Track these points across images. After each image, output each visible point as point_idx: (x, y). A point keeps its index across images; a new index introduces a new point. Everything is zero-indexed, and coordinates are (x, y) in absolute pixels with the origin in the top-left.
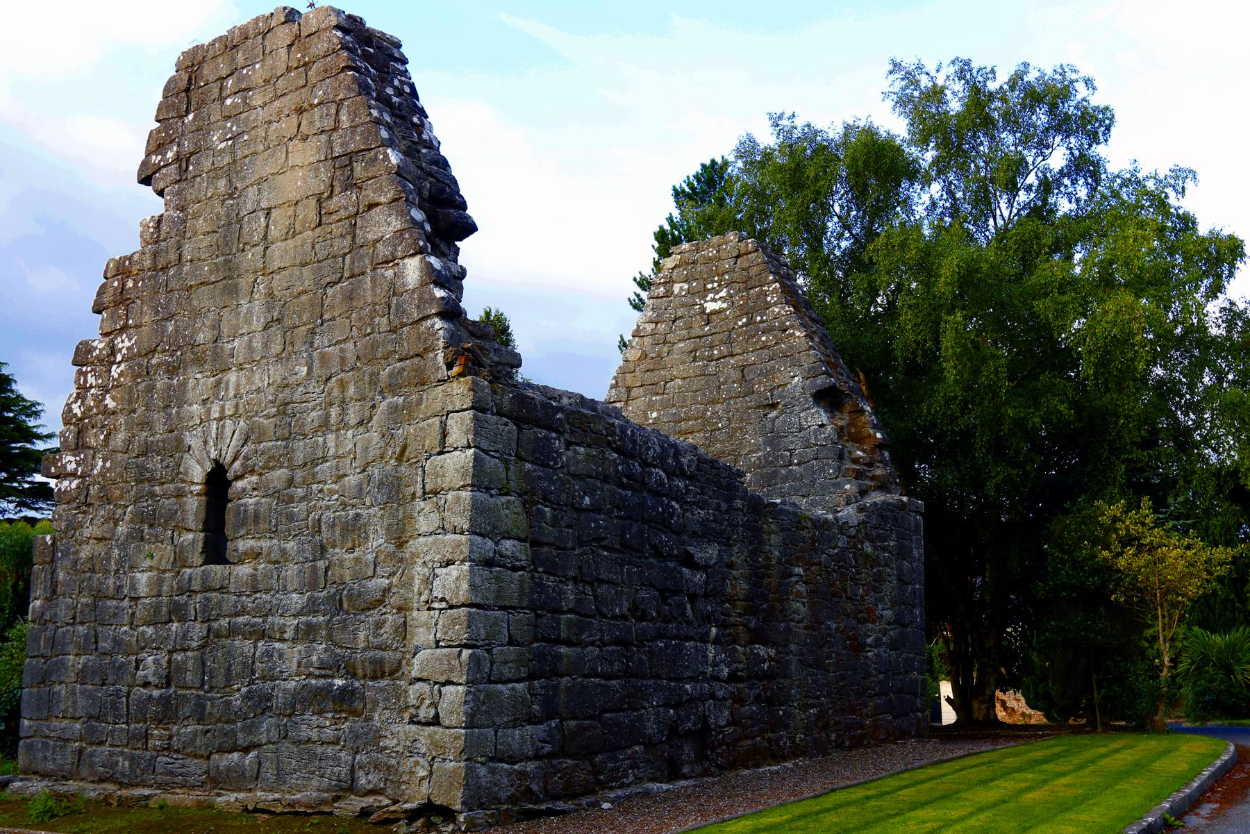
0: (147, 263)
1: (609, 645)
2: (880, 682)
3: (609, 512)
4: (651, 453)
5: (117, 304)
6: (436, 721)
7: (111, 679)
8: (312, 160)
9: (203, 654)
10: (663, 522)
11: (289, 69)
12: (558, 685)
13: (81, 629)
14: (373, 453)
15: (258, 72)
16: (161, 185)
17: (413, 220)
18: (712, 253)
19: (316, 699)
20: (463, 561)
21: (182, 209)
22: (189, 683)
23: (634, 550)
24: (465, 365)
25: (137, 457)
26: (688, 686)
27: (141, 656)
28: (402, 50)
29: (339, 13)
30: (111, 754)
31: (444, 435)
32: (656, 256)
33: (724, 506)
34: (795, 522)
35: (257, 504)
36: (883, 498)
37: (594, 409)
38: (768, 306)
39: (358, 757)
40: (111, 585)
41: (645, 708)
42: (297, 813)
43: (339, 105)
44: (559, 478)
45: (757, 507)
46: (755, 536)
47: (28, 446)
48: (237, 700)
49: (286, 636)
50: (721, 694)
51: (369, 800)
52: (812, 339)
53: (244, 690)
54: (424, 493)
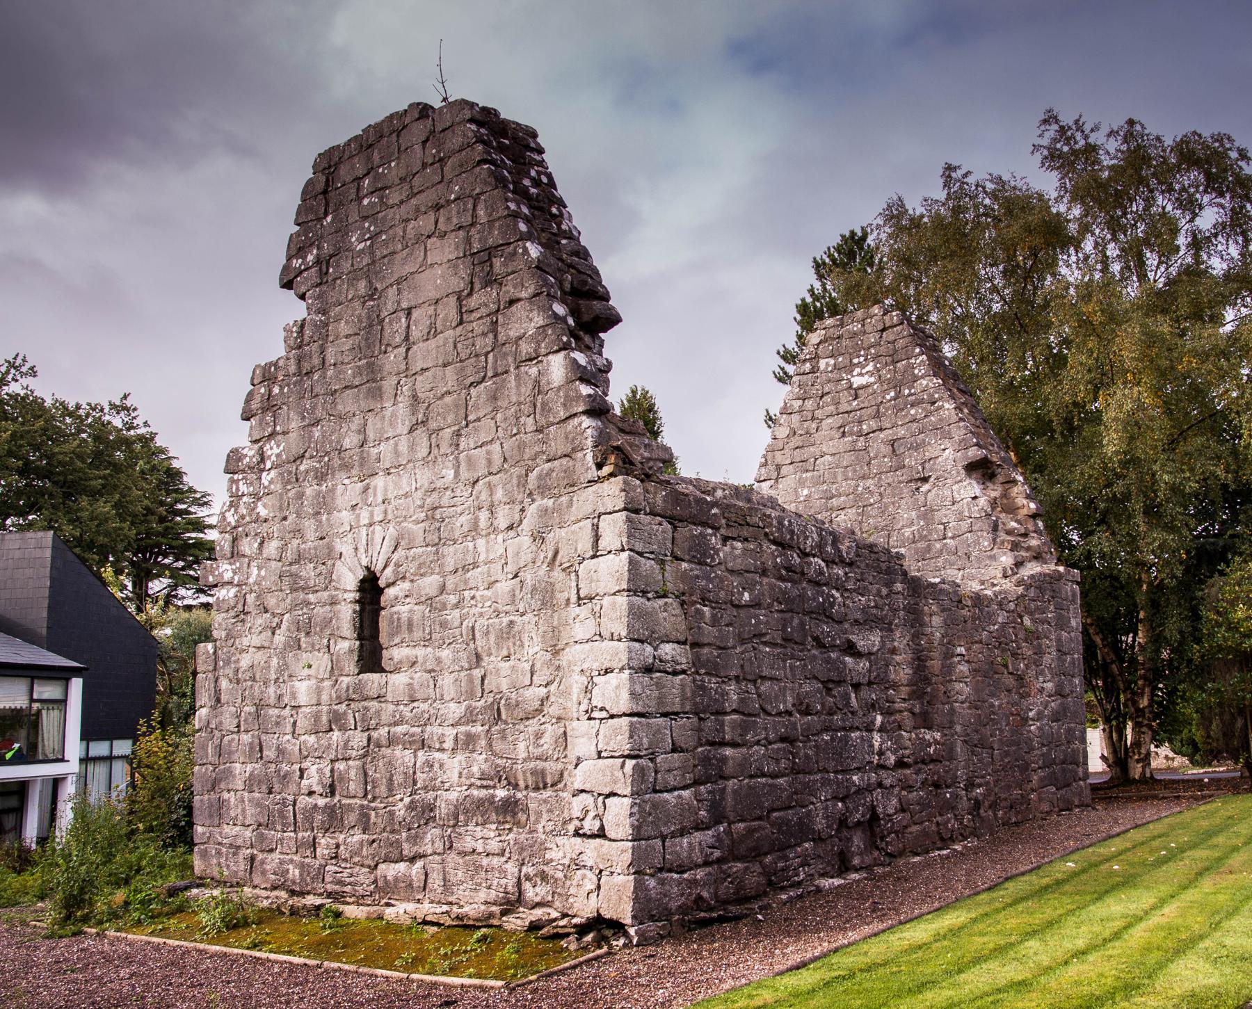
0: (292, 369)
1: (775, 742)
2: (1043, 755)
3: (770, 606)
4: (809, 542)
5: (264, 410)
6: (601, 834)
7: (277, 787)
8: (452, 257)
9: (365, 763)
10: (824, 613)
11: (424, 166)
12: (724, 788)
13: (246, 738)
14: (526, 557)
15: (393, 170)
16: (303, 289)
17: (555, 315)
18: (857, 327)
19: (479, 809)
20: (622, 669)
21: (324, 312)
22: (352, 793)
23: (796, 643)
24: (616, 465)
25: (291, 564)
26: (855, 778)
27: (304, 765)
28: (539, 140)
29: (472, 105)
30: (282, 862)
31: (597, 538)
32: (799, 328)
33: (884, 591)
34: (952, 598)
35: (410, 611)
36: (1039, 569)
37: (749, 500)
38: (916, 379)
39: (524, 869)
40: (273, 695)
41: (813, 803)
42: (466, 927)
43: (476, 199)
44: (717, 576)
45: (916, 587)
46: (916, 619)
47: (201, 535)
48: (400, 810)
49: (445, 746)
50: (888, 782)
51: (538, 913)
52: (961, 410)
53: (407, 800)
54: (579, 598)
